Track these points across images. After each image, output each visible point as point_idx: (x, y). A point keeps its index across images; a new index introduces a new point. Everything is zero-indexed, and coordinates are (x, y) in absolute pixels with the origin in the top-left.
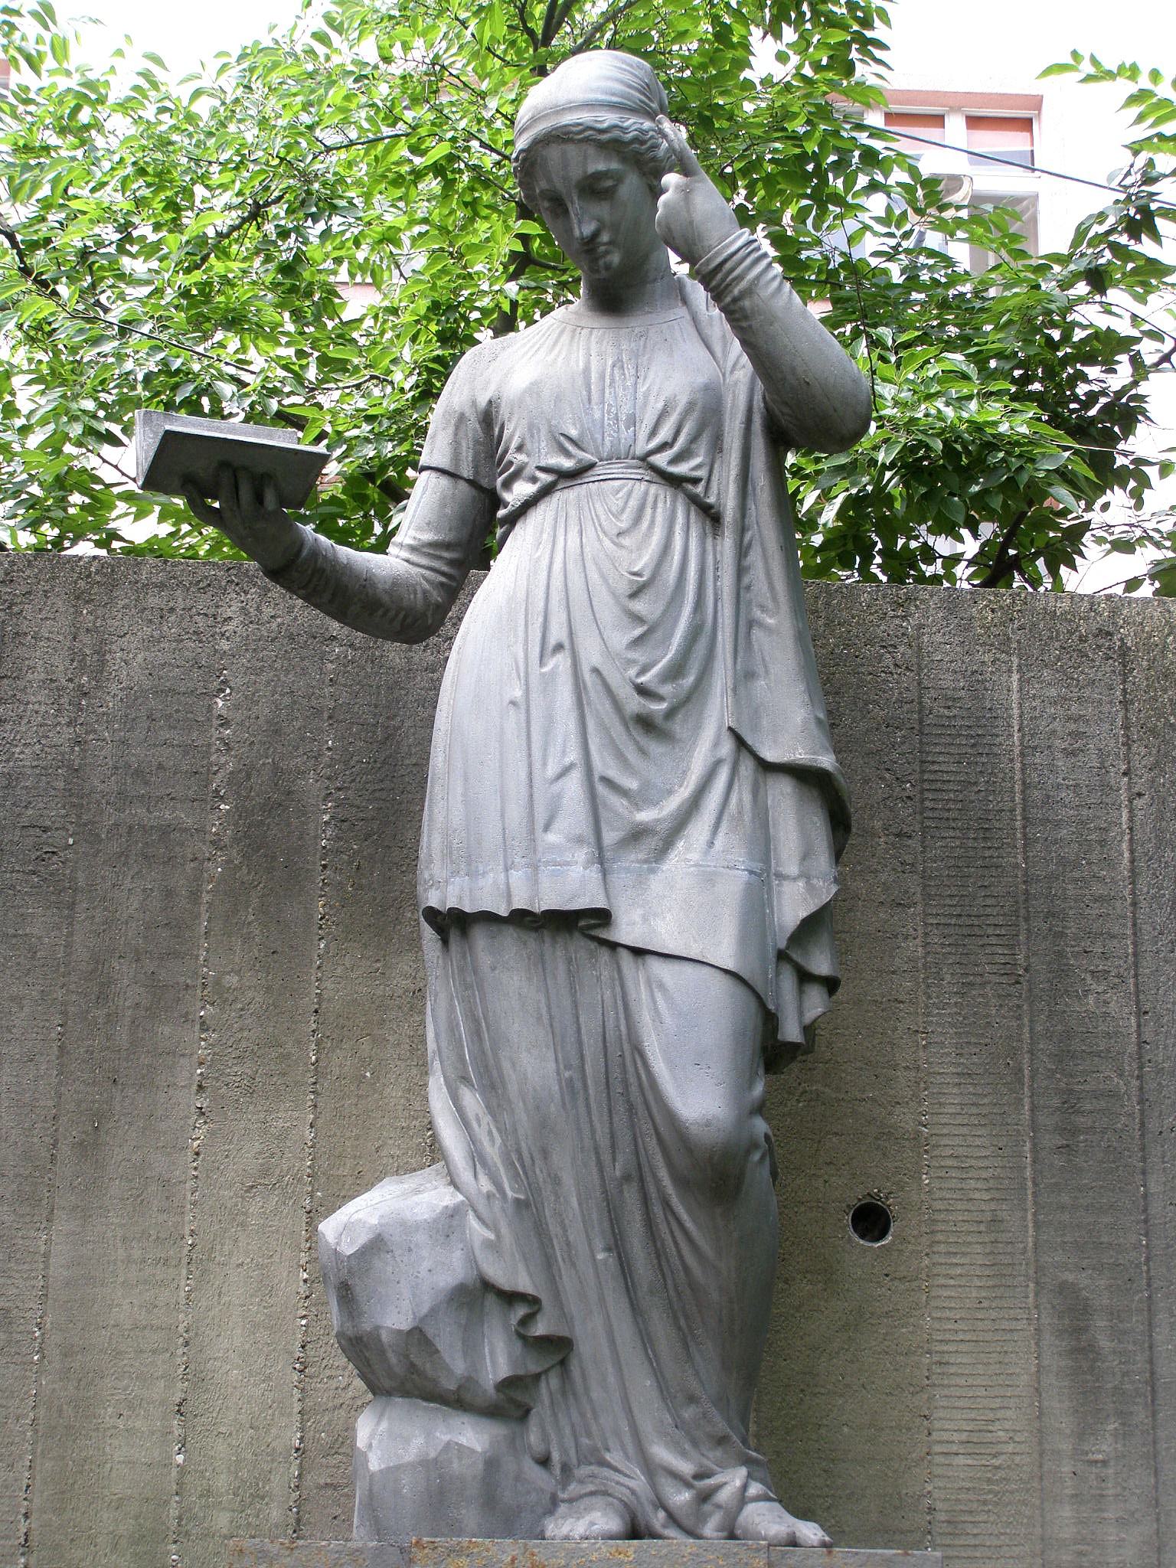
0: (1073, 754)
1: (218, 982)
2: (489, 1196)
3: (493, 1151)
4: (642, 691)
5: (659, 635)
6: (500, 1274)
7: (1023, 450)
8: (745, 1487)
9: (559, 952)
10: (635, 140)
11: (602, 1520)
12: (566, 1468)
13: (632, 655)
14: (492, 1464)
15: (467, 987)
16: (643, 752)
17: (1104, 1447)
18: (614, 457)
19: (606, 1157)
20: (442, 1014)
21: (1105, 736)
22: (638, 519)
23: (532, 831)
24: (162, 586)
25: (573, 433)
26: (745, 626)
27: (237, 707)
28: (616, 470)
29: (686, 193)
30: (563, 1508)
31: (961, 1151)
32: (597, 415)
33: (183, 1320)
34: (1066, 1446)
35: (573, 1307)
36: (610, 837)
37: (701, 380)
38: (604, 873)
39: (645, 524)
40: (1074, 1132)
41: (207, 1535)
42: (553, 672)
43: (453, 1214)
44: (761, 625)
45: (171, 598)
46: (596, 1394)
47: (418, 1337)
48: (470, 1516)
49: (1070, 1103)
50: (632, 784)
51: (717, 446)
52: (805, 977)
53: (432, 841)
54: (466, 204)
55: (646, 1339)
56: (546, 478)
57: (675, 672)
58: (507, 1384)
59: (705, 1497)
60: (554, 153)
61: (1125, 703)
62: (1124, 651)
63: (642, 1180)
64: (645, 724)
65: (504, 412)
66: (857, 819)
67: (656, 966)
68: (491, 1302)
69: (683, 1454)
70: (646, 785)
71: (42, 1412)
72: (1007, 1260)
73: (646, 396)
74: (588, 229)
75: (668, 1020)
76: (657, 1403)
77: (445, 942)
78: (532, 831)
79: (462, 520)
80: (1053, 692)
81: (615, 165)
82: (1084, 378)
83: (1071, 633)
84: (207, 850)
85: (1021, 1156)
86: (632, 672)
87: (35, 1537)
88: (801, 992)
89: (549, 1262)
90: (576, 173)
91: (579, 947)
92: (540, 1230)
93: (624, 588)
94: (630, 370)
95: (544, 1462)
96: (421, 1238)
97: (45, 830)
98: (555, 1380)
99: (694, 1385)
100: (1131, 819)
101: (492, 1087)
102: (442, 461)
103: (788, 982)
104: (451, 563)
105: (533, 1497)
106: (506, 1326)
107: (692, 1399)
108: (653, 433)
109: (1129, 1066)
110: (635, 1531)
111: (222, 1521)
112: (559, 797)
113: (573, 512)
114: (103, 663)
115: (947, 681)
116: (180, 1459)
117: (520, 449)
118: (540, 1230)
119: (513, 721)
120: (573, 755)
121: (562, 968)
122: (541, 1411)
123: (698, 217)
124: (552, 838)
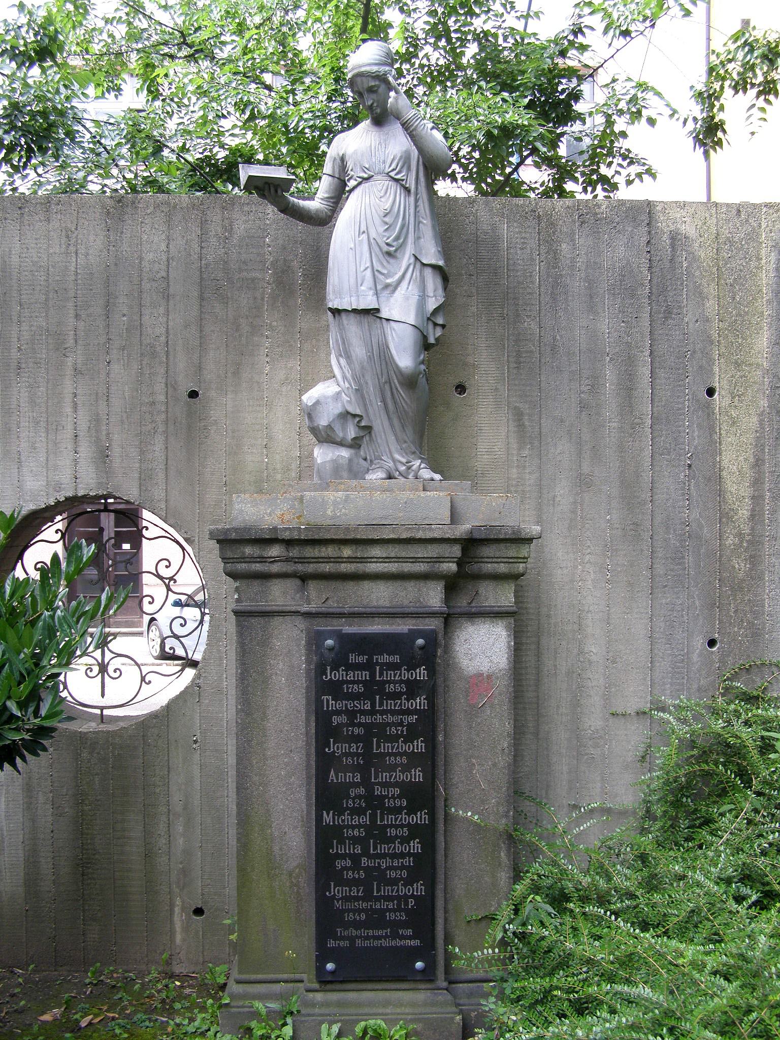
0: (523, 249)
1: (270, 324)
2: (348, 388)
3: (349, 376)
4: (388, 244)
5: (392, 228)
6: (351, 409)
7: (526, 129)
8: (420, 465)
9: (366, 320)
10: (383, 74)
11: (381, 474)
12: (371, 461)
13: (384, 234)
14: (350, 460)
15: (340, 329)
16: (388, 262)
17: (526, 452)
18: (379, 173)
19: (380, 377)
20: (334, 337)
21: (533, 243)
22: (386, 193)
23: (357, 286)
24: (248, 204)
25: (367, 166)
26: (417, 223)
27: (272, 241)
28: (379, 177)
29: (396, 99)
30: (371, 471)
31: (487, 369)
32: (374, 160)
33: (265, 422)
34: (515, 452)
35: (372, 417)
36: (379, 287)
37: (404, 149)
38: (378, 297)
39: (388, 194)
40: (520, 363)
41: (275, 480)
42: (362, 240)
43: (338, 393)
44: (422, 223)
45: (251, 207)
46: (379, 441)
47: (329, 427)
48: (345, 474)
49: (519, 354)
50: (386, 272)
51: (409, 169)
52: (435, 325)
53: (330, 288)
54: (344, 14)
55: (392, 425)
56: (360, 180)
57: (397, 238)
58: (354, 439)
59: (409, 468)
60: (359, 80)
61: (539, 233)
62: (539, 216)
63: (390, 383)
64: (389, 254)
65: (347, 158)
66: (451, 278)
67: (392, 323)
68: (349, 417)
69: (403, 457)
70: (389, 272)
71: (227, 448)
72: (499, 400)
73: (388, 154)
74: (370, 103)
75: (396, 339)
76: (396, 443)
77: (334, 316)
78: (357, 286)
79: (336, 190)
80: (517, 230)
81: (377, 83)
82: (562, 83)
83: (523, 211)
84: (266, 285)
85: (504, 370)
86: (385, 239)
87: (227, 482)
88: (434, 328)
89: (365, 405)
90: (366, 86)
91: (371, 318)
92: (363, 397)
93: (382, 214)
94: (383, 146)
95: (365, 459)
96: (329, 400)
97: (218, 280)
98: (367, 438)
99: (406, 438)
100: (539, 269)
101: (348, 357)
102: (330, 173)
103: (431, 326)
104: (333, 203)
105: (362, 469)
106: (354, 424)
107: (405, 442)
108: (390, 166)
109: (537, 343)
110: (390, 477)
111: (279, 477)
112: (364, 276)
113: (367, 191)
114: (232, 228)
115: (485, 227)
116: (266, 460)
117: (352, 170)
118: (363, 397)
119: (351, 253)
120: (368, 264)
121: (366, 324)
122: (364, 446)
123: (400, 107)
124: (363, 288)
